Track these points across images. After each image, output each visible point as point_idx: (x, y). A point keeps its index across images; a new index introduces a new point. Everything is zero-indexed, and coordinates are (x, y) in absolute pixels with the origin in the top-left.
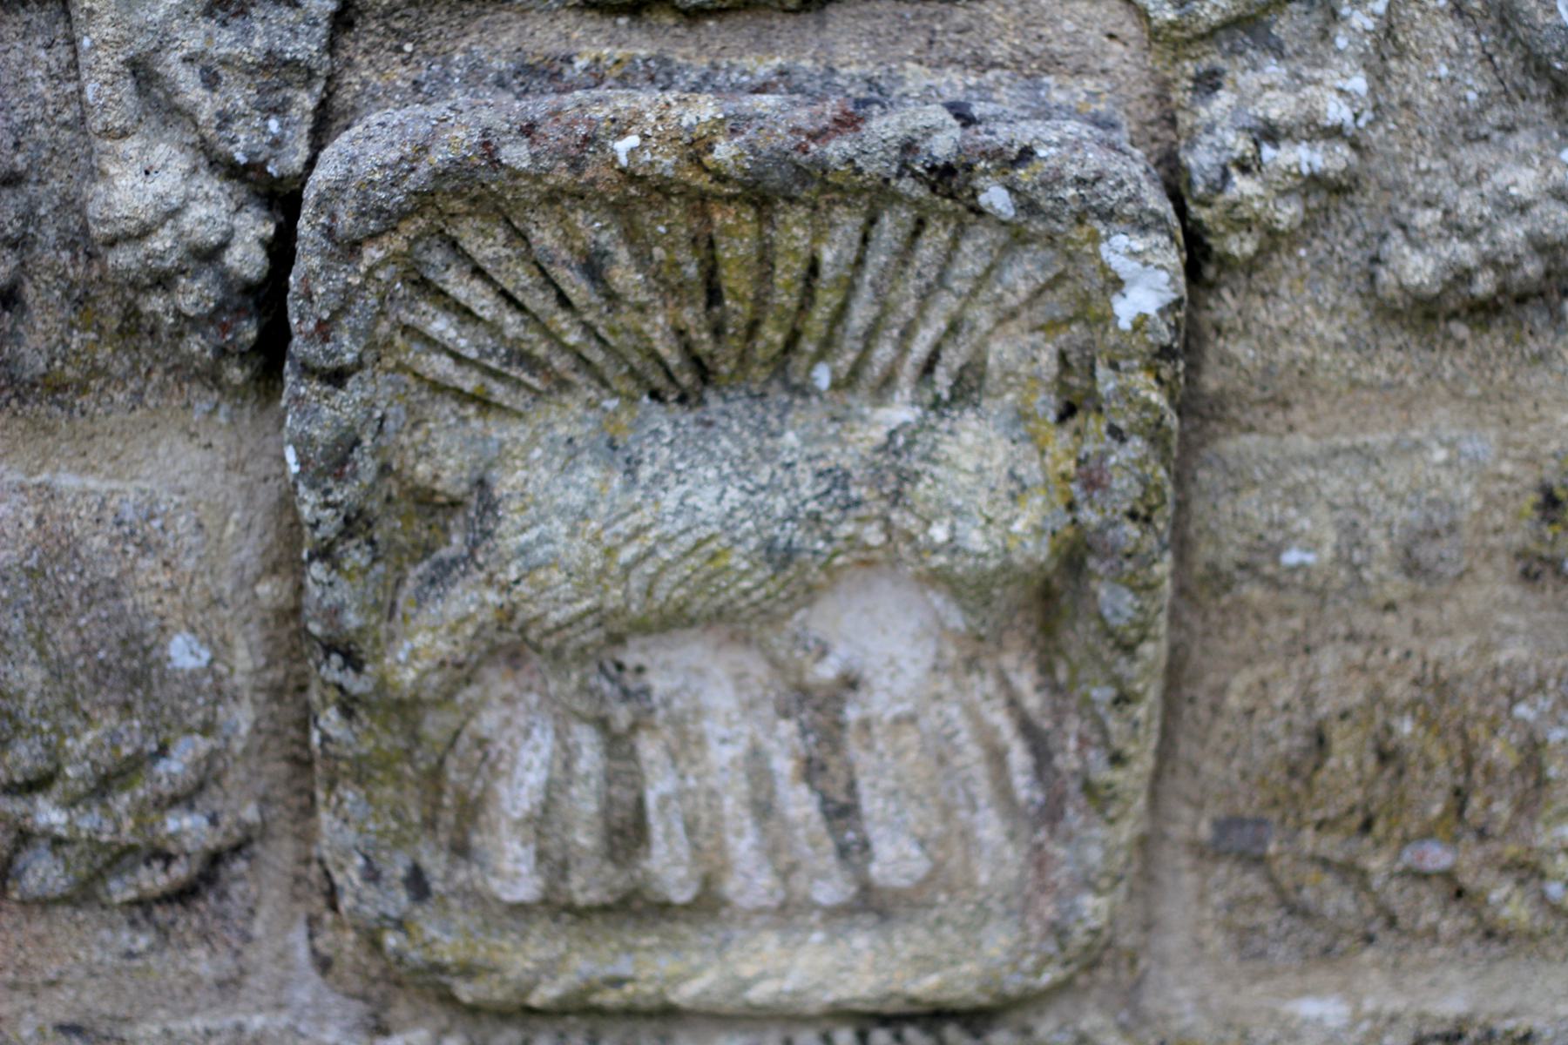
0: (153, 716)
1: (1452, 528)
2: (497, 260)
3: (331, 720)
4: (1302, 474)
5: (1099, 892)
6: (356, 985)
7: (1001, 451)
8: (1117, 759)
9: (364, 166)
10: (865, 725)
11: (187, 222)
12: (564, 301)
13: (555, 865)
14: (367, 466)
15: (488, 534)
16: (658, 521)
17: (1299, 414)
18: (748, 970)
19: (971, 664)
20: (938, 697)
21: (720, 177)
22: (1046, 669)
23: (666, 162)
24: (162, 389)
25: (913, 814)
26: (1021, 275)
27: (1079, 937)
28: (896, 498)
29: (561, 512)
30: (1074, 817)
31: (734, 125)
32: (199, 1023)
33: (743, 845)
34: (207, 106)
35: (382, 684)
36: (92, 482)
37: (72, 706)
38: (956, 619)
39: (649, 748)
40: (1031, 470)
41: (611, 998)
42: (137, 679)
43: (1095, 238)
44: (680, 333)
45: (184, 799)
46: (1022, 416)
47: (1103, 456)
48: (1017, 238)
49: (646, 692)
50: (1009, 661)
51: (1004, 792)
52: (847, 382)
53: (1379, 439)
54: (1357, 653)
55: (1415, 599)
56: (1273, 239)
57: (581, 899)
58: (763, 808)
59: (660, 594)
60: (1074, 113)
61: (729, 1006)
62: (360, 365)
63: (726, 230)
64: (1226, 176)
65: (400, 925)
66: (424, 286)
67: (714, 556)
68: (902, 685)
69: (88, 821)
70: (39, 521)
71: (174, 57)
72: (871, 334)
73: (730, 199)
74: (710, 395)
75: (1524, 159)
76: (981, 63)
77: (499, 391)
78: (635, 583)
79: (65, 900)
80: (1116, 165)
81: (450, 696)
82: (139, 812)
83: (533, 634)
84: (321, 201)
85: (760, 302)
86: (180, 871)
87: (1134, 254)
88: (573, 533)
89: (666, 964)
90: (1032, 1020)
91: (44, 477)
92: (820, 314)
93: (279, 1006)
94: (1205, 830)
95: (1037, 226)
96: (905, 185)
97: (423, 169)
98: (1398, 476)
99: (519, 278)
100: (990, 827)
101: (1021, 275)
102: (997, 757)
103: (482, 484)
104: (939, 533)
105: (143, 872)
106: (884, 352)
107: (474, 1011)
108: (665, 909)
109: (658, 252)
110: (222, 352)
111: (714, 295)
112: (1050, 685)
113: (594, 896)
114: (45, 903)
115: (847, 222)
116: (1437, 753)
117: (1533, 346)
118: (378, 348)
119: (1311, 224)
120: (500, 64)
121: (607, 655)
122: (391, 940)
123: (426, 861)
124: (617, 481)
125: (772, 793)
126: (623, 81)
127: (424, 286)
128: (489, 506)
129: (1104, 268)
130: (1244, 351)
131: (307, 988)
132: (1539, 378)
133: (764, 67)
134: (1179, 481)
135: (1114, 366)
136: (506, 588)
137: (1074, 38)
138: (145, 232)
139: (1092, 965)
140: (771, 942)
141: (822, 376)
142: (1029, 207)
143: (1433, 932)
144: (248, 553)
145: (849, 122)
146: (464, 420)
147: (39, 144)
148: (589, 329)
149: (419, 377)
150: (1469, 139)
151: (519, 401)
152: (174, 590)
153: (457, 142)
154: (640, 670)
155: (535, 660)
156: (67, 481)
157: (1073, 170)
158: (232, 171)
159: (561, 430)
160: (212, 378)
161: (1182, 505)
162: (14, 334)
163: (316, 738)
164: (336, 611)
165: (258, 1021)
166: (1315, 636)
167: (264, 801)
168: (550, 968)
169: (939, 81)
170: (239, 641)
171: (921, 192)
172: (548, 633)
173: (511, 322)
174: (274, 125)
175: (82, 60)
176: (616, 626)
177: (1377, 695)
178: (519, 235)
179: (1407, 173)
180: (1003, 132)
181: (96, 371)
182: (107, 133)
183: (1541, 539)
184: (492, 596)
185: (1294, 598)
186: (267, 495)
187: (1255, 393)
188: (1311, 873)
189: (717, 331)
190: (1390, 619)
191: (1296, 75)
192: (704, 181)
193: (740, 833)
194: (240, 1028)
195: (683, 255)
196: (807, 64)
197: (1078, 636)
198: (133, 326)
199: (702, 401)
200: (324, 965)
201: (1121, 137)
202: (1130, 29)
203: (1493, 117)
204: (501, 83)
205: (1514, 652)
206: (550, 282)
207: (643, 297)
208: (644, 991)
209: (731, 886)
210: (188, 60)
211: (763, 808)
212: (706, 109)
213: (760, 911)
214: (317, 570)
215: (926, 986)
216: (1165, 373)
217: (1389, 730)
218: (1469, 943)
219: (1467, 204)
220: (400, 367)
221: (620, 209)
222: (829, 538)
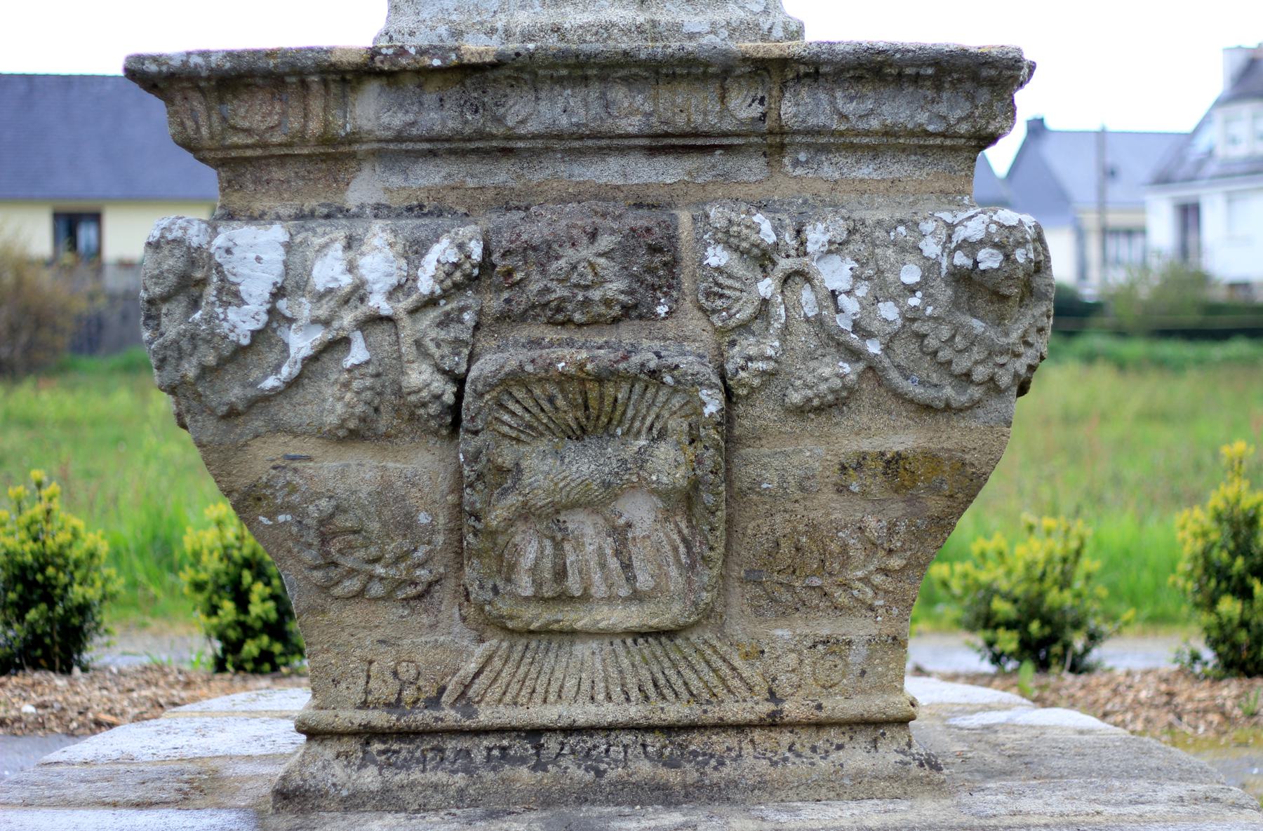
0: (413, 539)
1: (814, 476)
2: (523, 398)
3: (470, 538)
4: (766, 460)
5: (708, 592)
6: (474, 626)
7: (672, 453)
8: (711, 549)
9: (486, 372)
10: (634, 539)
11: (432, 388)
12: (542, 410)
13: (538, 584)
14: (484, 459)
15: (519, 479)
16: (571, 475)
17: (764, 442)
18: (599, 618)
19: (666, 520)
20: (656, 530)
21: (588, 374)
22: (690, 521)
23: (573, 370)
24: (420, 437)
25: (649, 567)
26: (677, 402)
27: (702, 606)
28: (641, 468)
29: (542, 472)
30: (699, 568)
31: (592, 359)
32: (423, 639)
33: (597, 577)
34: (436, 353)
35: (486, 526)
36: (398, 465)
37: (388, 535)
38: (660, 505)
39: (567, 547)
40: (681, 459)
41: (556, 627)
42: (408, 527)
43: (697, 391)
44: (577, 419)
45: (421, 565)
46: (679, 443)
47: (703, 454)
48: (675, 391)
49: (566, 529)
50: (678, 518)
51: (678, 561)
52: (626, 433)
53: (789, 449)
54: (787, 516)
55: (804, 499)
56: (753, 390)
57: (546, 595)
58: (603, 566)
59: (571, 497)
60: (692, 353)
61: (592, 630)
62: (483, 429)
63: (590, 389)
64: (737, 371)
65: (490, 603)
66: (502, 406)
67: (587, 485)
68: (645, 526)
69: (392, 572)
70: (382, 477)
71: (428, 339)
72: (633, 419)
73: (591, 380)
74: (585, 437)
75: (827, 365)
76: (665, 339)
77: (523, 437)
78: (564, 493)
79: (382, 598)
80: (703, 369)
81: (507, 530)
82: (408, 569)
83: (533, 510)
84: (473, 382)
85: (600, 410)
86: (419, 588)
87: (708, 395)
88: (545, 479)
89: (573, 616)
90: (690, 636)
91: (384, 464)
92: (618, 413)
93: (449, 633)
94: (743, 574)
95: (680, 387)
96: (642, 376)
97: (503, 372)
98: (795, 460)
99: (529, 403)
100: (674, 572)
101: (677, 402)
102: (675, 549)
103: (517, 464)
104: (654, 478)
105: (408, 589)
106: (637, 424)
107: (512, 632)
108: (572, 598)
109: (570, 396)
110: (441, 426)
111: (587, 408)
112: (691, 526)
113: (550, 594)
114: (376, 599)
115: (625, 387)
116: (814, 548)
117: (835, 420)
118: (488, 424)
119: (764, 385)
120: (523, 340)
121: (554, 517)
122: (487, 608)
123: (498, 583)
124: (558, 463)
125: (606, 561)
126: (560, 345)
127: (502, 406)
128: (520, 471)
129: (700, 399)
130: (745, 422)
131: (458, 627)
132: (837, 430)
133: (601, 341)
134: (727, 461)
135: (704, 428)
136: (525, 496)
137: (693, 331)
138: (420, 390)
139: (708, 617)
140: (606, 609)
141: (619, 431)
142: (678, 382)
143: (817, 606)
144: (445, 487)
145: (625, 358)
146: (512, 445)
147: (386, 364)
148: (550, 418)
149: (499, 433)
150: (813, 359)
151: (528, 439)
152: (422, 498)
153: (513, 364)
154: (565, 522)
155: (533, 518)
156: (391, 465)
157: (690, 371)
158: (444, 372)
159: (541, 448)
160: (436, 433)
161: (728, 470)
162: (377, 420)
163: (465, 543)
164: (473, 503)
165: (442, 638)
166: (774, 511)
167: (446, 566)
168: (537, 617)
169: (652, 344)
170: (441, 514)
171: (646, 378)
172: (537, 509)
173: (527, 416)
174: (456, 359)
175: (401, 340)
176: (558, 507)
177: (794, 529)
178: (530, 391)
179: (793, 369)
180: (670, 360)
181: (401, 432)
182: (408, 362)
183: (842, 480)
184: (521, 498)
185: (766, 499)
186: (451, 469)
187: (750, 435)
188: (777, 587)
189: (588, 418)
190: (797, 505)
191: (758, 341)
192: (583, 375)
193: (595, 573)
194: (436, 641)
195: (577, 396)
196: (614, 340)
197: (698, 510)
198: (413, 417)
199: (583, 439)
200: (464, 619)
201: (706, 360)
202: (709, 328)
203: (819, 352)
204: (523, 346)
205: (836, 515)
206: (538, 404)
207: (566, 409)
208: (565, 624)
209: (593, 591)
210: (432, 340)
211: (603, 566)
212: (584, 355)
213: (602, 599)
214: (468, 490)
215: (654, 622)
216: (719, 430)
217: (799, 541)
218: (830, 611)
219: (810, 379)
220: (494, 430)
221: (559, 383)
222: (621, 480)
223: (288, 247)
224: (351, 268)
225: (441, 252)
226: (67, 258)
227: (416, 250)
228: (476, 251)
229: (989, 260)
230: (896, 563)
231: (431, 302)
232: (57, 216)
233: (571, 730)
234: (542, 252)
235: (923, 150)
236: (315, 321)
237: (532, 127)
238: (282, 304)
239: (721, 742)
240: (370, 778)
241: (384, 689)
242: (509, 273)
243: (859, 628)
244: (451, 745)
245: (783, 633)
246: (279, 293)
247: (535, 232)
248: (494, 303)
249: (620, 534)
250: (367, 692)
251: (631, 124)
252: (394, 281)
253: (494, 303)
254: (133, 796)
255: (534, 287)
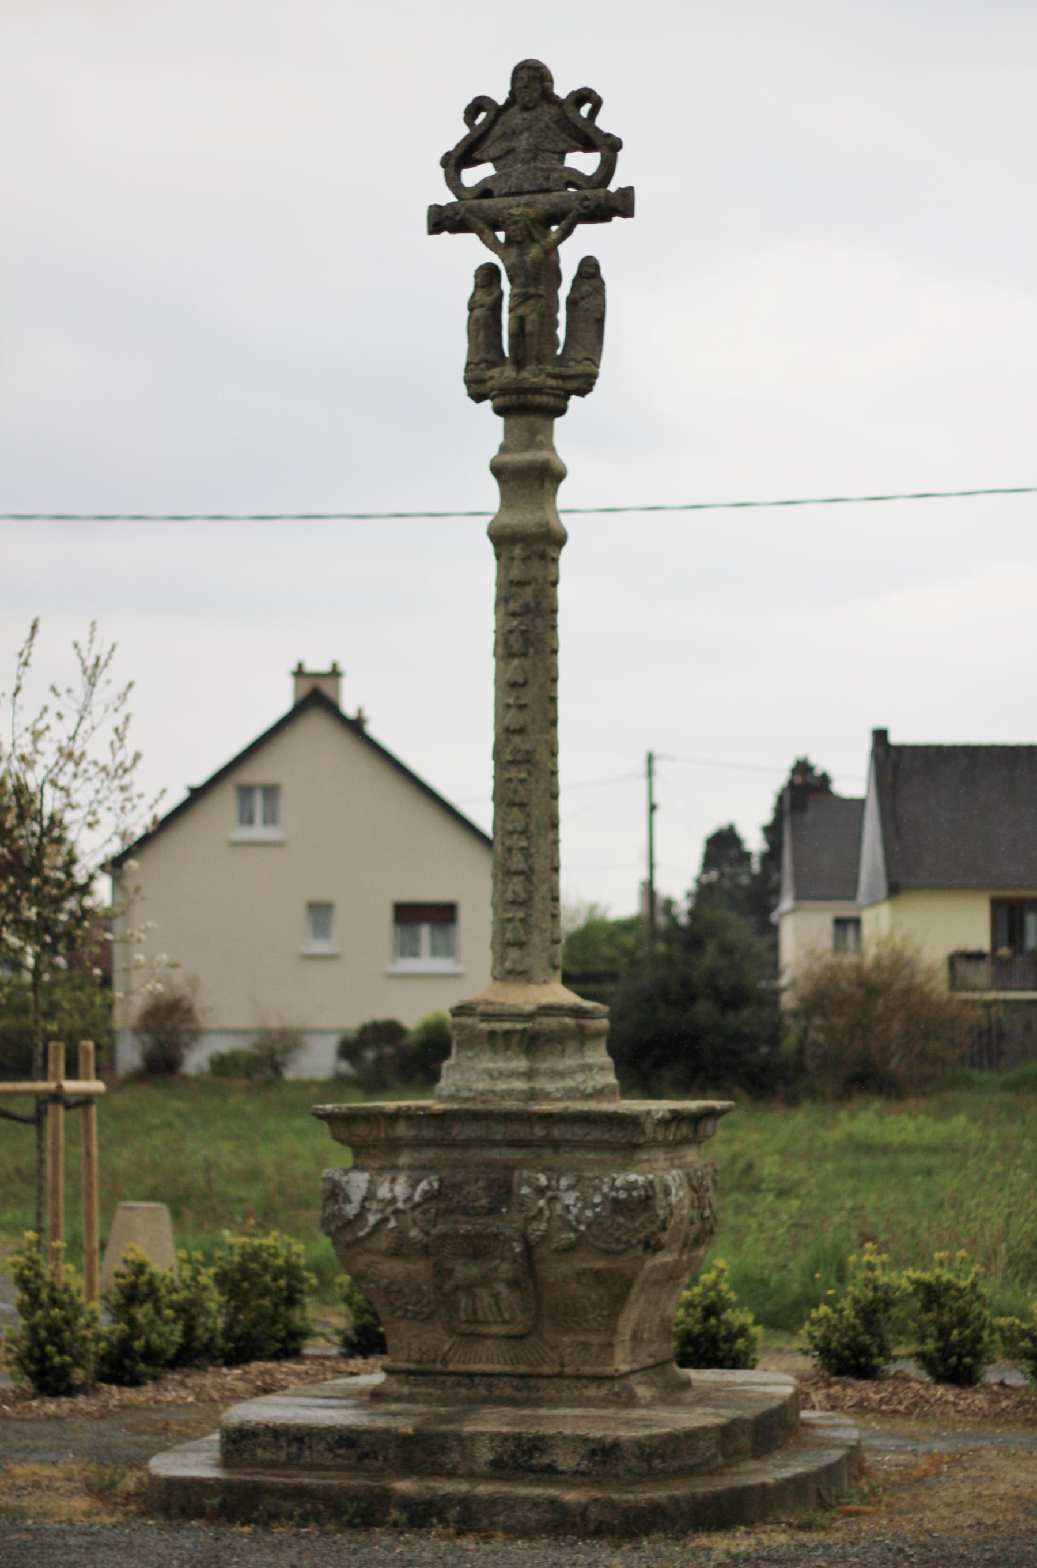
223: (370, 1182)
224: (392, 1190)
225: (423, 1186)
226: (1004, 951)
227: (414, 1185)
228: (436, 1185)
229: (623, 1195)
230: (605, 1313)
231: (418, 1205)
232: (996, 905)
233: (484, 1375)
234: (458, 1187)
235: (614, 1149)
236: (378, 1211)
237: (462, 1137)
238: (367, 1204)
239: (542, 1383)
240: (405, 1390)
241: (415, 1355)
242: (447, 1194)
243: (596, 1339)
244: (440, 1379)
245: (566, 1339)
246: (365, 1199)
247: (459, 1178)
248: (442, 1206)
249: (496, 1296)
250: (409, 1355)
251: (498, 1137)
252: (406, 1196)
253: (442, 1206)
254: (328, 1394)
255: (455, 1200)
